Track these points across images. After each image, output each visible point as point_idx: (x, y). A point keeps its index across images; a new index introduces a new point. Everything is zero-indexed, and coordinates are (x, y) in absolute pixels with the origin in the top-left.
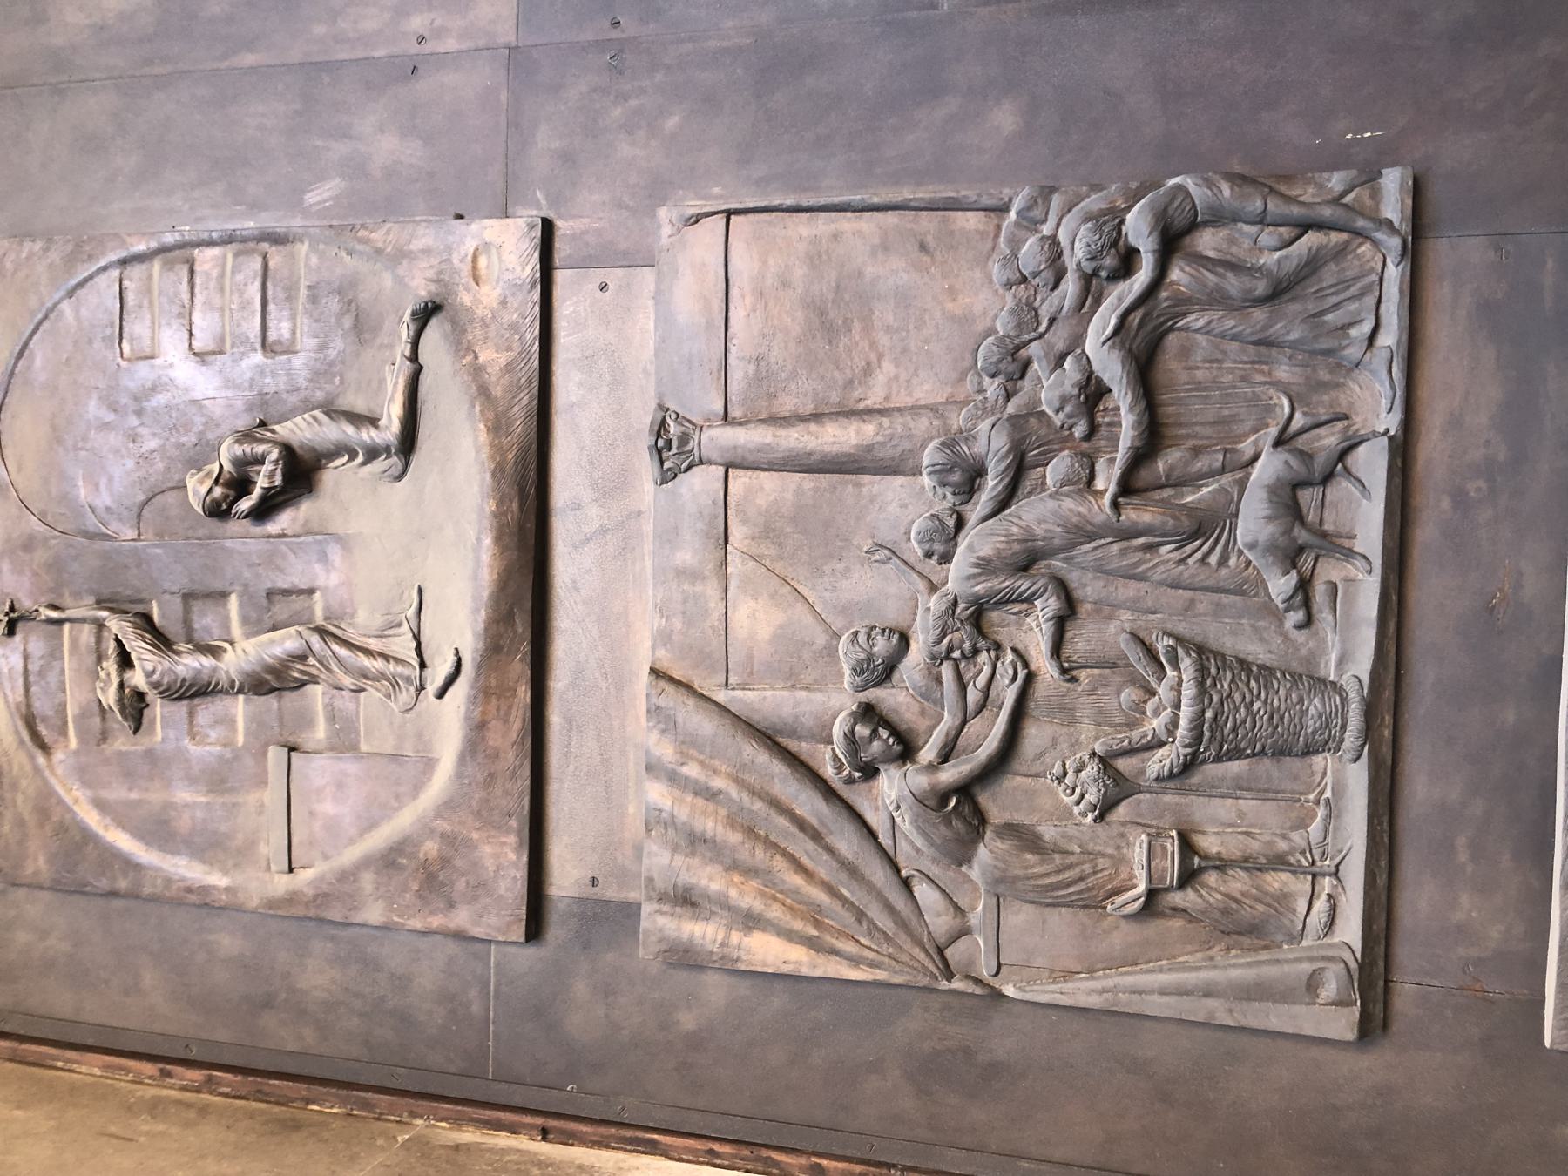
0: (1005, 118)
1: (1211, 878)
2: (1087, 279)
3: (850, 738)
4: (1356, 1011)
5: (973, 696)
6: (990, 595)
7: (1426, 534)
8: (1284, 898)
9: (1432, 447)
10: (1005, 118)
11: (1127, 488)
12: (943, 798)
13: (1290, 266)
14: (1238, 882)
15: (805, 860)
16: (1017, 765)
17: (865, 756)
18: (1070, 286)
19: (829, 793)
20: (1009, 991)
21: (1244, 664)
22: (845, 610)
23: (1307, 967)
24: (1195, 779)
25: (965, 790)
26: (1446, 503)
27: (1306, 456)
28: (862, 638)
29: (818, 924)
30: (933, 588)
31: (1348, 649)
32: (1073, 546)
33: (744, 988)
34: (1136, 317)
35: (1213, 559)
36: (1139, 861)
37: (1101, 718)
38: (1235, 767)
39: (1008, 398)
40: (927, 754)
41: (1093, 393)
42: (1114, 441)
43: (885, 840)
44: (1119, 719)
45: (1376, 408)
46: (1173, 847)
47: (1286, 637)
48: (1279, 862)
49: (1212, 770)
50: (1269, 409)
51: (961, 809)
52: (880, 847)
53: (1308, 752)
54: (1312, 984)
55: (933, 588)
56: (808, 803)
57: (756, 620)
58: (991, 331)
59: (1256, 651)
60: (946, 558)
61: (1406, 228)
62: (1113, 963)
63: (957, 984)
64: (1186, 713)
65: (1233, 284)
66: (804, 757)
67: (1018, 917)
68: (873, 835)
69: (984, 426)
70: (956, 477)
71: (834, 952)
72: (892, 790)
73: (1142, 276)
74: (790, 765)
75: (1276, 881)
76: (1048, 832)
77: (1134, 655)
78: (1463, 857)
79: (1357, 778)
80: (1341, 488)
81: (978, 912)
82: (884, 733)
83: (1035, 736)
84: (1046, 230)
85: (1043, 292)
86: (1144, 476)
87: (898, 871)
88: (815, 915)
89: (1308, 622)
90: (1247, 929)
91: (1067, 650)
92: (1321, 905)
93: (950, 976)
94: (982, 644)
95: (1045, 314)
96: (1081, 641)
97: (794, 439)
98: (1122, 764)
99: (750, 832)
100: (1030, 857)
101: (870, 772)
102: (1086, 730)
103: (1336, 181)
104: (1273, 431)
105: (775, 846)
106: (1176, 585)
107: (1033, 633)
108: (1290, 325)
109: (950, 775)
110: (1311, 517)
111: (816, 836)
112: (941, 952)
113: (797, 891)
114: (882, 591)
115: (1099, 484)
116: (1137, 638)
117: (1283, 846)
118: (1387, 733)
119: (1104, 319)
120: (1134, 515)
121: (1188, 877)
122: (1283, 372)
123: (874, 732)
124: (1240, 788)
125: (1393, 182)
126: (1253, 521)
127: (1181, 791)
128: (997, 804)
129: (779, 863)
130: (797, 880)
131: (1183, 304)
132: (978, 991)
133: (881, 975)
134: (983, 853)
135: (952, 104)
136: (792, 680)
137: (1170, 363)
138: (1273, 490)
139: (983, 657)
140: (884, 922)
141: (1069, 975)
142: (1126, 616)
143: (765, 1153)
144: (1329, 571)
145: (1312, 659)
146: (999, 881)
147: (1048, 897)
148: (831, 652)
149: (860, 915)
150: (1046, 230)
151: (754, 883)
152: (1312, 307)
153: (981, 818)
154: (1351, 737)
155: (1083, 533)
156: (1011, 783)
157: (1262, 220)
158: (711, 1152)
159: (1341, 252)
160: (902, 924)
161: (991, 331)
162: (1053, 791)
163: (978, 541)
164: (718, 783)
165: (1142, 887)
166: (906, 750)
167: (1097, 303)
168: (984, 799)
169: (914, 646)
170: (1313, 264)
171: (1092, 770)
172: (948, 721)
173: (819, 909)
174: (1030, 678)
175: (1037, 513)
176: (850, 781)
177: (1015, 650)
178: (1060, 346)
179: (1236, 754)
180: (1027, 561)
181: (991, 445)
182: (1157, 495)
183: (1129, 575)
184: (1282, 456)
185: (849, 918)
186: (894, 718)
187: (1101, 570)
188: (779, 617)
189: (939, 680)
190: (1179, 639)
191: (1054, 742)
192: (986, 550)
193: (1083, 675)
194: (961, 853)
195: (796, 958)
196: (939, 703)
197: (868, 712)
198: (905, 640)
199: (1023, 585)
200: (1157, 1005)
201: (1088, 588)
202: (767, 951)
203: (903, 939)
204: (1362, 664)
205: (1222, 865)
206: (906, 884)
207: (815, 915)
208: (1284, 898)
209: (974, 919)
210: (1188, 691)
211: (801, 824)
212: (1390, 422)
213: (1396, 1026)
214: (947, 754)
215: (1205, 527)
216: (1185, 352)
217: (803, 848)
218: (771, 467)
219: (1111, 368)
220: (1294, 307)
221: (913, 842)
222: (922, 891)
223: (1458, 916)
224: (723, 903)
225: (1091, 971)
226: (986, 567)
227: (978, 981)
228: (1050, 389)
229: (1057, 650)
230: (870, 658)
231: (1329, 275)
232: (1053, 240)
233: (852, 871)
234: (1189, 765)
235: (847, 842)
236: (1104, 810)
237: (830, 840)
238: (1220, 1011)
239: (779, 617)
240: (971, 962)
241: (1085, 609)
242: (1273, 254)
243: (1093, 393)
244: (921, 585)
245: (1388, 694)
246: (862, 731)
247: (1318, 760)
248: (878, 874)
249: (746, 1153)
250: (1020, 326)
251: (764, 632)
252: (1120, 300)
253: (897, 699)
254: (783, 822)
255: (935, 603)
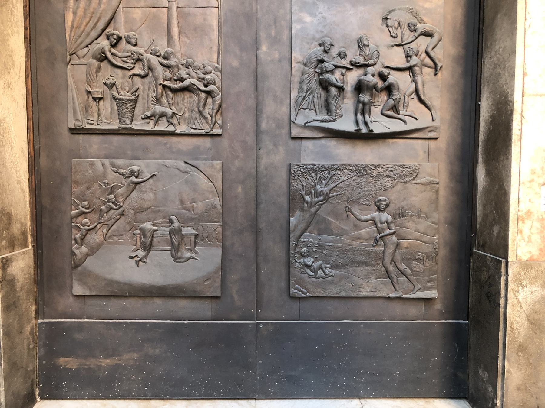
0: (235, 63)
1: (95, 103)
2: (203, 79)
3: (113, 34)
4: (74, 127)
5: (125, 59)
6: (144, 62)
7: (160, 139)
8: (93, 116)
9: (174, 139)
10: (235, 63)
11: (164, 86)
12: (104, 53)
13: (205, 114)
14: (95, 108)
15: (89, 25)
16: (112, 68)
17: (110, 37)
18: (202, 76)
19: (103, 30)
20: (69, 67)
21: (135, 108)
22: (140, 34)
23: (80, 119)
24: (113, 100)
25: (106, 58)
26: (165, 142)
27: (172, 117)
28: (134, 37)
29: (76, 28)
30: (146, 51)
31: (138, 125)
32: (154, 77)
33: (61, 12)
34: (195, 87)
35: (153, 102)
36: (97, 90)
37: (123, 83)
38: (116, 107)
39: (182, 65)
40: (113, 50)
41: (182, 80)
42: (174, 84)
43: (95, 42)
44: (123, 86)
45: (182, 128)
46: (100, 96)
47: (139, 116)
48: (99, 115)
49: (115, 103)
50: (180, 112)
51: (102, 57)
52: (93, 41)
53: (119, 119)
54: (77, 120)
55: (146, 51)
56: (101, 25)
57: (137, 14)
58: (194, 61)
59: (136, 111)
60: (151, 54)
61: (211, 133)
62: (77, 86)
63: (68, 57)
64: (124, 97)
65: (202, 104)
66: (110, 25)
67: (84, 69)
68: (96, 39)
69: (176, 60)
70: (166, 55)
71: (71, 31)
72: (104, 43)
73: (202, 88)
74: (109, 20)
75: (96, 115)
76: (100, 74)
77: (135, 89)
78: (104, 146)
79: (116, 127)
80: (166, 124)
81: (83, 61)
82: (115, 41)
83: (119, 71)
84: (213, 71)
85: (202, 71)
86: (167, 90)
87: (90, 44)
88: (78, 27)
89: (143, 119)
90: (86, 110)
91: (135, 77)
92: (92, 122)
93: (71, 55)
94: (135, 61)
95: (198, 71)
96: (137, 79)
97: (175, 22)
98: (114, 87)
99: (93, 13)
100: (95, 70)
101: (108, 39)
102: (121, 81)
103: (220, 122)
104: (176, 112)
105: (91, 19)
106: (148, 96)
107: (138, 70)
108: (196, 115)
109: (109, 55)
110: (161, 119)
111: (94, 27)
112: (75, 53)
113: (82, 23)
114: (145, 41)
115: (166, 82)
116: (138, 89)
117: (102, 116)
118: (124, 132)
119: (195, 81)
120: (160, 87)
121: (94, 99)
122: (187, 114)
123: (115, 39)
124: (112, 109)
125: (219, 131)
126: (159, 109)
127: (111, 98)
128: (104, 64)
129: (88, 19)
130: (84, 24)
131: (198, 96)
132: (68, 61)
133: (68, 41)
134: (95, 61)
135: (238, 52)
136: (126, 22)
137: (187, 95)
138: (165, 112)
139: (132, 61)
140: (79, 41)
141: (73, 78)
142: (142, 88)
143: (28, 17)
144: (152, 123)
145: (136, 120)
146: (89, 64)
147: (88, 74)
148: (132, 31)
149: (80, 37)
150: (213, 71)
151: (82, 14)
152: (198, 118)
153: (102, 61)
154: (122, 126)
155: (156, 79)
156: (109, 66)
157: (213, 109)
158: (26, 6)
159: (207, 123)
160: (79, 45)
161: (194, 61)
162: (108, 74)
163: (154, 60)
164: (102, 6)
165: (91, 90)
166: (114, 46)
167: (200, 81)
168: (105, 62)
169: (134, 47)
170: (205, 118)
171: (113, 82)
172: (120, 54)
173: (80, 27)
174: (129, 70)
175: (160, 70)
176: (106, 35)
177: (134, 67)
178: (191, 74)
179: (118, 107)
180: (150, 68)
181: (172, 62)
182: (164, 92)
183: (149, 88)
184: (171, 113)
185: (78, 34)
186: (119, 43)
187: (150, 82)
188: (138, 19)
189: (127, 52)
190: (138, 96)
191: (117, 75)
192: (152, 61)
193: (130, 80)
194: (94, 57)
195: (69, 23)
196: (123, 53)
197: (119, 38)
198: (135, 45)
199: (146, 68)
200: (70, 94)
201: (147, 80)
202: (69, 17)
203: (76, 46)
204: (135, 127)
205: (98, 105)
206: (87, 46)
207: (78, 27)
208: (93, 116)
209: (82, 60)
210: (128, 98)
211: (96, 24)
212: (178, 131)
213: (73, 136)
214: (112, 54)
215: (158, 101)
216: (190, 97)
217: (91, 24)
218: (168, 17)
219: (186, 83)
220: (198, 115)
221: (95, 48)
222: (86, 50)
223: (93, 145)
224: (78, 8)
225: (75, 82)
226: (149, 61)
227: (70, 61)
228: (183, 73)
229: (134, 75)
230: (130, 38)
231: (203, 121)
232: (211, 73)
233: (88, 35)
234: (115, 99)
235: (94, 34)
236: (105, 84)
237: (93, 30)
238: (70, 105)
239: (138, 19)
240: (73, 59)
241: (143, 80)
242: (207, 111)
243: (182, 80)
244: (146, 49)
245: (130, 132)
246: (115, 37)
247: (118, 121)
248: (88, 41)
249: (28, 13)
250: (195, 67)
251: (135, 16)
252: (199, 84)
253: (123, 44)
254: (96, 20)
255: (142, 51)
